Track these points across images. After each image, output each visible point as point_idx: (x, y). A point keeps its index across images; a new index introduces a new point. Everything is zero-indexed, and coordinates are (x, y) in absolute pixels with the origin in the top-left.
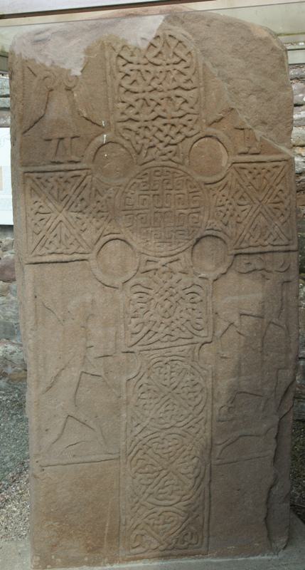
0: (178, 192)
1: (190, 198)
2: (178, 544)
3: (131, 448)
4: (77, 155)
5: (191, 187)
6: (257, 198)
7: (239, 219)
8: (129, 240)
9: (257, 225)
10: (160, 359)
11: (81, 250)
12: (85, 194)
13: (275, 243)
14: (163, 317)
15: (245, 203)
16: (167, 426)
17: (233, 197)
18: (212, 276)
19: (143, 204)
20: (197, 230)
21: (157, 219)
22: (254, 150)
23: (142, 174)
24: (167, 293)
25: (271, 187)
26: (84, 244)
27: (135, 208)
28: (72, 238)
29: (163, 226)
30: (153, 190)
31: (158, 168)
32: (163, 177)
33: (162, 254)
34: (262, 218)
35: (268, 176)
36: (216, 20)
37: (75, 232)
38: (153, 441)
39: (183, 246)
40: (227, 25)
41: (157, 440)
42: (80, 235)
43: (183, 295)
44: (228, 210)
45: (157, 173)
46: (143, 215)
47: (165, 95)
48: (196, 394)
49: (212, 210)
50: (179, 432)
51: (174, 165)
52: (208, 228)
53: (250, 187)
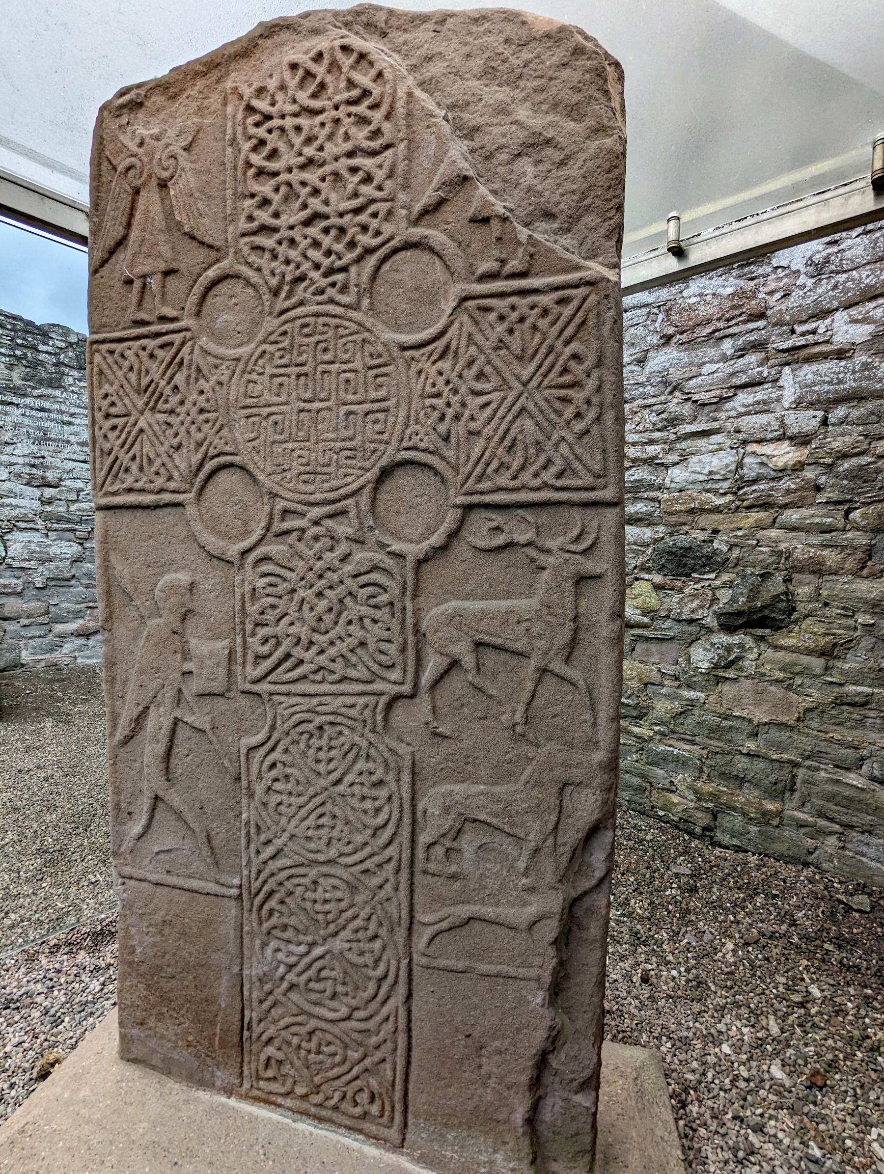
0: (344, 367)
1: (370, 379)
2: (344, 1106)
3: (258, 884)
4: (174, 308)
5: (371, 355)
6: (518, 377)
7: (473, 426)
8: (251, 467)
9: (515, 439)
10: (305, 716)
11: (172, 485)
12: (180, 379)
13: (559, 483)
14: (314, 631)
15: (487, 386)
16: (321, 857)
17: (460, 376)
18: (414, 550)
19: (278, 395)
20: (382, 447)
21: (303, 425)
22: (514, 264)
23: (276, 334)
24: (323, 582)
25: (551, 349)
26: (176, 474)
27: (263, 401)
28: (158, 462)
29: (312, 439)
30: (297, 365)
31: (307, 320)
32: (317, 338)
33: (312, 498)
34: (529, 424)
35: (543, 323)
36: (452, 15)
37: (161, 450)
38: (296, 881)
39: (354, 481)
40: (476, 20)
41: (302, 880)
42: (170, 456)
43: (354, 588)
44: (449, 405)
45: (306, 330)
46: (279, 417)
47: (328, 169)
48: (377, 804)
49: (414, 406)
50: (345, 876)
51: (339, 310)
52: (405, 444)
53: (503, 352)
